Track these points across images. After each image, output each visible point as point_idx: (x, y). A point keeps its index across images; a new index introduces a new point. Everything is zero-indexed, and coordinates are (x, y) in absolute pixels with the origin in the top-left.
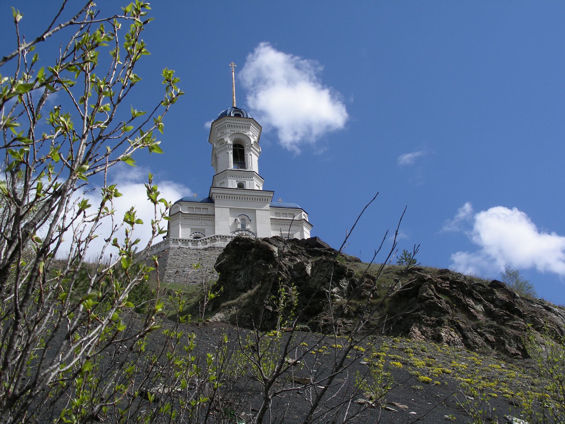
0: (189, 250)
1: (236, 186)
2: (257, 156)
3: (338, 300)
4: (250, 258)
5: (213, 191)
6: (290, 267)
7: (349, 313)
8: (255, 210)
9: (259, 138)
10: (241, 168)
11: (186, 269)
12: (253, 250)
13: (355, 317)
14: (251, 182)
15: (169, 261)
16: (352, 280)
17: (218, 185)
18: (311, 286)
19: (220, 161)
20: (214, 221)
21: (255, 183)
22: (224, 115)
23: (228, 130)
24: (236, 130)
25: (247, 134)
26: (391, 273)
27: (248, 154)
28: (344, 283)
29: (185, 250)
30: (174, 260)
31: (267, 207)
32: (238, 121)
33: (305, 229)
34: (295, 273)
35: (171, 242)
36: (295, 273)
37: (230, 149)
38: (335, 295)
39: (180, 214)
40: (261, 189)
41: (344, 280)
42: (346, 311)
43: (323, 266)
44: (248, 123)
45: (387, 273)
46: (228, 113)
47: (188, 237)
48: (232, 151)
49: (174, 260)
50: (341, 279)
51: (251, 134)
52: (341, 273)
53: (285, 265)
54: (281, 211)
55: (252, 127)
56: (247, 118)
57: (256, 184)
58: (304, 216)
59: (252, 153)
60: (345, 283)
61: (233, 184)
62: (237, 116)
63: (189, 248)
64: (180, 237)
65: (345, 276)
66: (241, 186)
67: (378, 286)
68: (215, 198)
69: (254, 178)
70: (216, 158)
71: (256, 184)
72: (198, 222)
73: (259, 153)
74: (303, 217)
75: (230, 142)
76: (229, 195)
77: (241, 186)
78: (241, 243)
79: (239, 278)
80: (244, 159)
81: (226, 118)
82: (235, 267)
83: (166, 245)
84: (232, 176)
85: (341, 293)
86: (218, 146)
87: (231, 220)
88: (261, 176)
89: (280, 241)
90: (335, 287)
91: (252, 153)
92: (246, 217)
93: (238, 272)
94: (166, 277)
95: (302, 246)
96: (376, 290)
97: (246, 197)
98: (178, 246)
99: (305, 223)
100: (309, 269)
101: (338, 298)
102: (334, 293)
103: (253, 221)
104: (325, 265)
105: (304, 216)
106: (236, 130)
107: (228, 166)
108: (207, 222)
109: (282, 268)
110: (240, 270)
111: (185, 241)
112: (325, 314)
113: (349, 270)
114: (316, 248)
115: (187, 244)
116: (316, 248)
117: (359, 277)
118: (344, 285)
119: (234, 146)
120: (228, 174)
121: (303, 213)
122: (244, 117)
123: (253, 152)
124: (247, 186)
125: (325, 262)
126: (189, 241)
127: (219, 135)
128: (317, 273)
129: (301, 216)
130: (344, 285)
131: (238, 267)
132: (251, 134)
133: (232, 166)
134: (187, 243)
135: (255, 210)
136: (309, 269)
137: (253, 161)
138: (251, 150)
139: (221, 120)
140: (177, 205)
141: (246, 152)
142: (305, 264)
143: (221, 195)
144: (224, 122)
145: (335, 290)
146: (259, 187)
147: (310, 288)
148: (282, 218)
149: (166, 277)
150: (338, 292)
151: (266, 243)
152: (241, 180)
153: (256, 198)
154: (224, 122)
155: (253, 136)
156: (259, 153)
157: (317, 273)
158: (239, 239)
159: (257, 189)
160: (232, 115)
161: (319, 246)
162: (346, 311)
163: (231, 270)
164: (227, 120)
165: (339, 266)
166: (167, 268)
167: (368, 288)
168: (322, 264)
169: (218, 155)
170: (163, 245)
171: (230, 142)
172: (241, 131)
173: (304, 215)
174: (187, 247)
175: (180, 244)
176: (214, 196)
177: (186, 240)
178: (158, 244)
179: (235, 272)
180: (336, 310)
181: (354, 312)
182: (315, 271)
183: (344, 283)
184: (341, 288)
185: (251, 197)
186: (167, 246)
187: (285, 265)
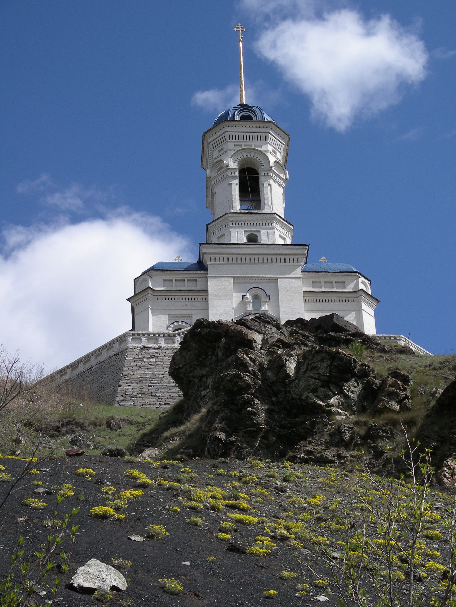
0: (159, 351)
1: (245, 240)
2: (281, 186)
3: (338, 417)
4: (220, 354)
5: (204, 250)
6: (261, 364)
7: (352, 438)
8: (277, 278)
9: (286, 156)
10: (256, 208)
11: (155, 383)
12: (224, 340)
13: (362, 445)
14: (270, 232)
15: (126, 371)
16: (368, 382)
17: (215, 240)
18: (294, 396)
19: (218, 199)
20: (207, 300)
21: (277, 233)
22: (225, 118)
23: (230, 145)
24: (244, 144)
25: (263, 149)
26: (446, 369)
27: (266, 184)
28: (353, 389)
29: (153, 352)
30: (134, 369)
31: (298, 272)
32: (248, 128)
33: (364, 306)
34: (269, 374)
35: (130, 339)
36: (269, 374)
37: (235, 177)
38: (333, 409)
39: (150, 291)
40: (289, 242)
41: (353, 382)
42: (347, 436)
43: (315, 360)
44: (261, 130)
45: (440, 368)
46: (230, 115)
47: (164, 330)
48: (237, 181)
49: (134, 369)
50: (347, 381)
51: (270, 148)
52: (345, 370)
53: (253, 361)
54: (322, 277)
55: (272, 137)
56: (263, 121)
57: (280, 235)
58: (363, 284)
59: (271, 182)
60: (353, 389)
61: (238, 236)
62: (244, 118)
63: (160, 348)
64: (151, 329)
65: (354, 375)
66: (253, 239)
67: (412, 391)
68: (208, 262)
69: (274, 225)
70: (213, 194)
71: (280, 235)
72: (180, 304)
73: (286, 181)
74: (361, 286)
75: (233, 165)
76: (233, 254)
77: (253, 239)
78: (205, 330)
79: (205, 389)
80: (259, 196)
81: (226, 123)
82: (199, 372)
83: (122, 345)
84: (237, 224)
85: (347, 405)
86: (214, 174)
87: (236, 298)
88: (289, 220)
89: (269, 323)
90: (335, 395)
91: (271, 182)
92: (261, 290)
93: (204, 379)
94: (119, 397)
95: (310, 331)
96: (407, 397)
97: (261, 257)
98: (141, 345)
99: (363, 297)
100: (291, 367)
101: (340, 414)
102: (332, 406)
103: (272, 297)
104: (319, 357)
105: (363, 284)
106: (244, 144)
107: (231, 207)
108: (195, 303)
109: (247, 367)
110: (207, 376)
111: (154, 337)
112: (310, 443)
113: (362, 365)
114: (332, 333)
115: (157, 341)
116: (332, 333)
117: (381, 377)
118: (352, 392)
119: (242, 171)
120: (230, 219)
121: (362, 279)
122: (257, 121)
123: (274, 181)
124: (264, 240)
125: (318, 352)
126: (159, 335)
127: (216, 154)
128: (305, 372)
129: (357, 284)
130: (352, 392)
131: (204, 372)
132: (270, 148)
133: (237, 206)
134: (157, 340)
135: (277, 279)
136: (291, 367)
137: (275, 196)
138: (270, 177)
139: (218, 128)
140: (144, 276)
141: (262, 181)
142: (284, 357)
143: (243, 257)
144: (223, 131)
145: (333, 401)
146: (284, 239)
147: (293, 399)
148: (323, 289)
149: (119, 397)
150: (340, 405)
151: (240, 328)
152: (253, 229)
153: (279, 257)
154: (223, 131)
155: (273, 151)
156: (286, 181)
157: (305, 372)
158: (202, 323)
159: (282, 242)
160: (237, 118)
161: (338, 328)
162: (347, 436)
163: (194, 377)
164: (228, 128)
165: (341, 359)
166: (121, 382)
167: (391, 395)
168: (314, 356)
169: (216, 190)
170: (116, 345)
171: (233, 165)
172: (253, 144)
173: (363, 282)
174: (157, 346)
175: (145, 342)
176: (206, 259)
177: (154, 335)
178: (110, 343)
179: (200, 380)
180: (330, 435)
181: (361, 437)
182: (303, 370)
183: (353, 389)
184: (346, 397)
185: (270, 257)
186: (123, 347)
187: (253, 361)
